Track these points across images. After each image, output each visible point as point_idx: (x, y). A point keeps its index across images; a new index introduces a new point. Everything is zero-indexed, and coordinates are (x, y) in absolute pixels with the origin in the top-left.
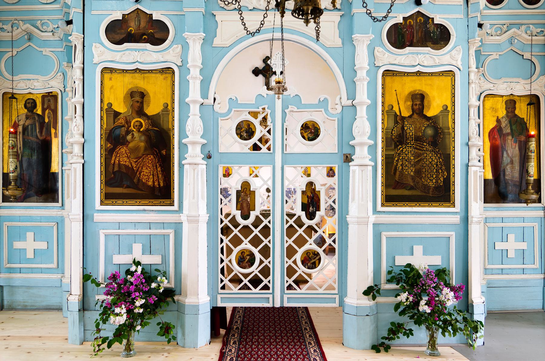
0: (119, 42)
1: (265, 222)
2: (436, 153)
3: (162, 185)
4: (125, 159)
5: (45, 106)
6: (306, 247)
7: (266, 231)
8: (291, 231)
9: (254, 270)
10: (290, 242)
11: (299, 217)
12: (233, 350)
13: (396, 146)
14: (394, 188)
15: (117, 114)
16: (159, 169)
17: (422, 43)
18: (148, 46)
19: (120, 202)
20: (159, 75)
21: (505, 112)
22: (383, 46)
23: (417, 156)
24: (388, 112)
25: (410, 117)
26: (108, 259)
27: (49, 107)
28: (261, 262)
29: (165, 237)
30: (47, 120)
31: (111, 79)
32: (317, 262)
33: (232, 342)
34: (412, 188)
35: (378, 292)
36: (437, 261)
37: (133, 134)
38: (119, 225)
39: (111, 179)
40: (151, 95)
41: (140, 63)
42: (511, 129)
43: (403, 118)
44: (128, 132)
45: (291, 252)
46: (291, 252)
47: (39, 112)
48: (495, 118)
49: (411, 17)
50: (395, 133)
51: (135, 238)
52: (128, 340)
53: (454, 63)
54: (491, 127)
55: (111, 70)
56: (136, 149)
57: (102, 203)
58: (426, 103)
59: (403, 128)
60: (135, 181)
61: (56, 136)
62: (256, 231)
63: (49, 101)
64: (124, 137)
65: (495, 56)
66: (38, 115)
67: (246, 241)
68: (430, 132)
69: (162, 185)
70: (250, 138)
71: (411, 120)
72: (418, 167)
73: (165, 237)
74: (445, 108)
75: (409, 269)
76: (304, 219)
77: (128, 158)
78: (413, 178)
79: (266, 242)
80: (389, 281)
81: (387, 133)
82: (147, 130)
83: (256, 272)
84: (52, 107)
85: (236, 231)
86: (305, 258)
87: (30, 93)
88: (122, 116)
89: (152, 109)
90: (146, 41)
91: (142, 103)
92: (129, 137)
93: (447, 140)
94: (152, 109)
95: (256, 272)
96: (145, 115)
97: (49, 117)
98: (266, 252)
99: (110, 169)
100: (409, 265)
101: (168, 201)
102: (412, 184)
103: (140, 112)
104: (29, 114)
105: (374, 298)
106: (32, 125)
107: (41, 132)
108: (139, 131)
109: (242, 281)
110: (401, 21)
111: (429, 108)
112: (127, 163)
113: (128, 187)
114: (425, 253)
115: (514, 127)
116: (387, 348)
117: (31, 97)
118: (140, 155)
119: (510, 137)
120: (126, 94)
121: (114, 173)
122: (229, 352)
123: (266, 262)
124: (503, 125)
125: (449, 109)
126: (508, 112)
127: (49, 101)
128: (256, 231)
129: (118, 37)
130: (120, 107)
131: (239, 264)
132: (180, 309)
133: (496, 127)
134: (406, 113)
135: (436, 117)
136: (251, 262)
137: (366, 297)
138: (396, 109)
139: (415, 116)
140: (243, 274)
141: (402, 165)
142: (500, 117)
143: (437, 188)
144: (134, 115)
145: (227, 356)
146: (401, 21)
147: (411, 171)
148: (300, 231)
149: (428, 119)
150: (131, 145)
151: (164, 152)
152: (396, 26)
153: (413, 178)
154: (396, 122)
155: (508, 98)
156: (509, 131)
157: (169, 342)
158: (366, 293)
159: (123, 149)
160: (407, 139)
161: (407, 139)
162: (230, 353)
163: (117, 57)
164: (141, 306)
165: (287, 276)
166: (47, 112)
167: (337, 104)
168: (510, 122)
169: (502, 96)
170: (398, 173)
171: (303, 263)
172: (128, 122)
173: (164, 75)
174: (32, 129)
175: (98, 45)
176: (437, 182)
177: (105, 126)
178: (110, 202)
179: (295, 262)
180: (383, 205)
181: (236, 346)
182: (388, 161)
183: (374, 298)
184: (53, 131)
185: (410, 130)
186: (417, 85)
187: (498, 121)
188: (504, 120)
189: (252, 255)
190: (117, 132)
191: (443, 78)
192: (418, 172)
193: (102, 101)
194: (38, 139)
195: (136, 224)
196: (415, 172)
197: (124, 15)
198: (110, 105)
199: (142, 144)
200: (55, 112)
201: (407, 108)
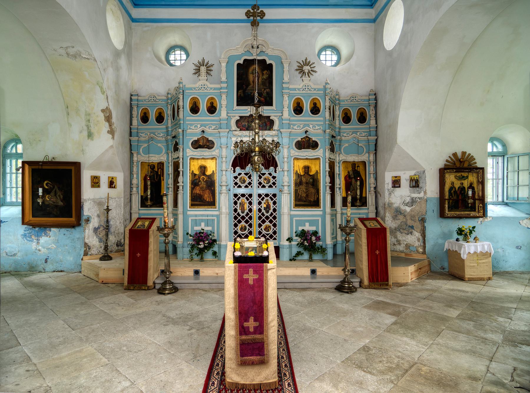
0: (196, 148)
1: (250, 214)
2: (314, 188)
3: (212, 201)
4: (198, 191)
5: (159, 168)
6: (266, 223)
7: (251, 218)
8: (260, 218)
9: (246, 232)
10: (260, 222)
11: (263, 212)
12: (220, 364)
13: (299, 186)
14: (298, 202)
15: (195, 175)
16: (211, 195)
17: (308, 147)
18: (207, 149)
19: (196, 207)
20: (210, 160)
21: (351, 169)
22: (293, 149)
23: (306, 189)
24: (296, 173)
25: (304, 175)
26: (192, 228)
27: (160, 168)
28: (249, 229)
29: (213, 220)
30: (159, 173)
31: (193, 162)
32: (270, 229)
33: (216, 372)
34: (305, 201)
35: (292, 239)
36: (314, 228)
37: (201, 182)
38: (196, 216)
39: (193, 199)
40: (208, 167)
41: (204, 156)
42: (354, 176)
43: (301, 176)
44: (199, 181)
45: (260, 226)
46: (260, 226)
47: (156, 170)
48: (347, 171)
49: (304, 138)
50: (298, 181)
51: (202, 220)
52: (202, 256)
53: (319, 155)
54: (346, 175)
55: (193, 159)
56: (203, 187)
57: (190, 208)
58: (310, 170)
59: (301, 179)
60: (202, 199)
61: (163, 180)
62: (247, 218)
63: (160, 165)
64: (198, 183)
65: (347, 145)
66: (156, 171)
67: (243, 222)
68: (311, 180)
69: (212, 201)
70: (244, 183)
71: (304, 176)
72: (307, 193)
73: (213, 220)
74: (317, 171)
75: (303, 231)
76: (265, 213)
77: (199, 191)
78: (305, 198)
79: (251, 222)
80: (296, 236)
81: (295, 181)
82: (206, 180)
83: (247, 233)
84: (162, 168)
85: (239, 218)
86: (265, 228)
87: (152, 162)
88: (197, 175)
89: (209, 173)
90: (206, 148)
91: (205, 170)
92: (200, 183)
93: (318, 184)
94: (209, 173)
95: (247, 233)
96: (206, 175)
97: (160, 172)
98: (250, 226)
99: (193, 195)
100: (303, 230)
101: (214, 207)
102: (305, 200)
103: (204, 174)
104: (152, 171)
105: (290, 242)
106: (153, 175)
107: (157, 178)
108: (203, 181)
109: (247, 217)
110: (300, 140)
111: (311, 172)
112: (199, 193)
113: (199, 201)
114: (310, 226)
115: (355, 175)
116: (295, 260)
117: (153, 164)
118: (204, 190)
119: (353, 179)
120: (199, 167)
121: (194, 196)
122: (217, 366)
123: (251, 229)
124: (351, 174)
125: (318, 172)
126: (352, 168)
127: (160, 165)
128: (247, 218)
129: (196, 146)
130: (197, 172)
131: (240, 230)
132: (220, 246)
133: (347, 175)
134: (302, 174)
135: (313, 175)
136: (245, 230)
137: (288, 242)
138: (299, 172)
139: (306, 174)
140: (242, 234)
141: (301, 193)
142: (349, 171)
143: (314, 201)
144: (202, 175)
145: (218, 354)
146: (300, 140)
147: (304, 195)
148: (264, 218)
149: (311, 176)
150: (201, 186)
151: (213, 189)
152: (298, 141)
153: (305, 198)
154: (299, 177)
155: (352, 163)
156: (353, 176)
157: (216, 257)
158: (287, 240)
159: (198, 188)
160: (303, 183)
161: (303, 183)
162: (217, 367)
163: (195, 154)
164: (207, 243)
165: (252, 217)
166: (159, 170)
167: (197, 272)
168: (353, 173)
169: (350, 162)
170: (299, 196)
171: (265, 229)
172: (199, 178)
173: (213, 160)
174: (153, 177)
175: (189, 149)
176: (314, 199)
177: (191, 179)
178: (193, 207)
179: (261, 229)
180: (294, 208)
181: (223, 360)
182: (296, 191)
183: (290, 242)
184: (162, 178)
185: (304, 180)
186: (307, 163)
187: (348, 172)
188: (351, 172)
189: (245, 227)
190: (195, 181)
191: (316, 160)
192: (307, 196)
193: (190, 170)
194: (155, 181)
195: (202, 215)
196: (306, 196)
197: (198, 138)
198: (193, 171)
199: (205, 186)
200: (163, 170)
201: (303, 172)
